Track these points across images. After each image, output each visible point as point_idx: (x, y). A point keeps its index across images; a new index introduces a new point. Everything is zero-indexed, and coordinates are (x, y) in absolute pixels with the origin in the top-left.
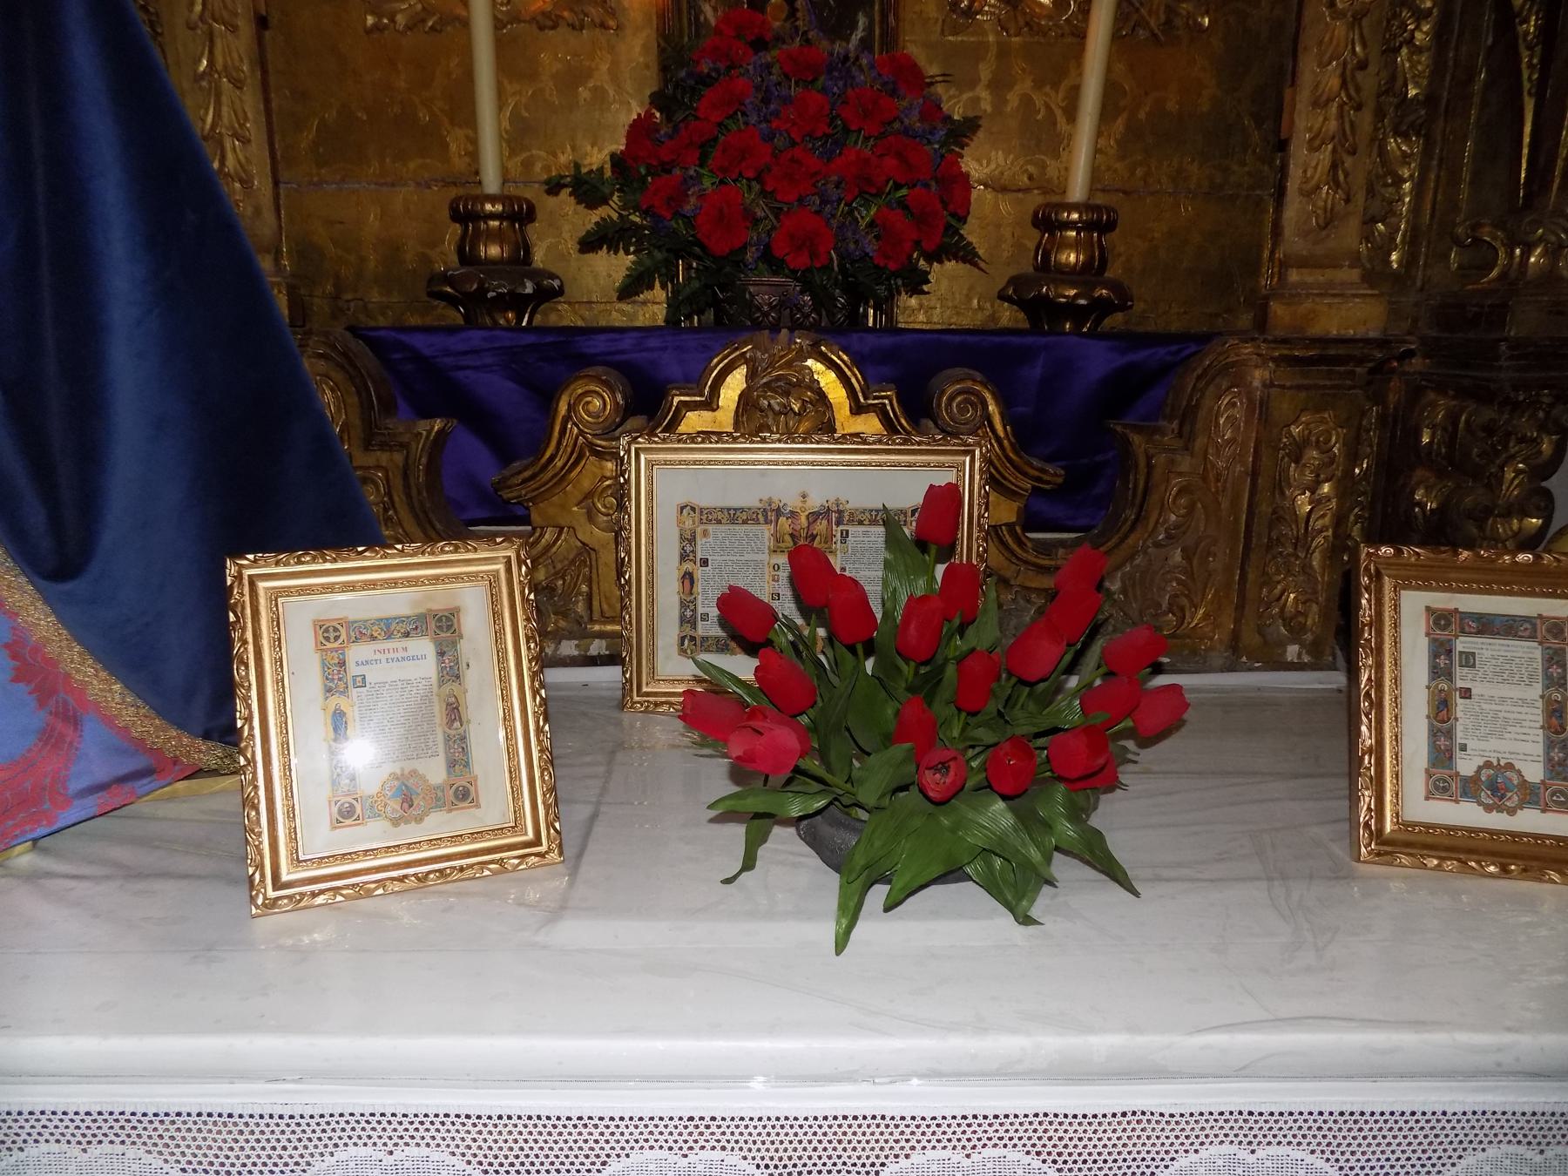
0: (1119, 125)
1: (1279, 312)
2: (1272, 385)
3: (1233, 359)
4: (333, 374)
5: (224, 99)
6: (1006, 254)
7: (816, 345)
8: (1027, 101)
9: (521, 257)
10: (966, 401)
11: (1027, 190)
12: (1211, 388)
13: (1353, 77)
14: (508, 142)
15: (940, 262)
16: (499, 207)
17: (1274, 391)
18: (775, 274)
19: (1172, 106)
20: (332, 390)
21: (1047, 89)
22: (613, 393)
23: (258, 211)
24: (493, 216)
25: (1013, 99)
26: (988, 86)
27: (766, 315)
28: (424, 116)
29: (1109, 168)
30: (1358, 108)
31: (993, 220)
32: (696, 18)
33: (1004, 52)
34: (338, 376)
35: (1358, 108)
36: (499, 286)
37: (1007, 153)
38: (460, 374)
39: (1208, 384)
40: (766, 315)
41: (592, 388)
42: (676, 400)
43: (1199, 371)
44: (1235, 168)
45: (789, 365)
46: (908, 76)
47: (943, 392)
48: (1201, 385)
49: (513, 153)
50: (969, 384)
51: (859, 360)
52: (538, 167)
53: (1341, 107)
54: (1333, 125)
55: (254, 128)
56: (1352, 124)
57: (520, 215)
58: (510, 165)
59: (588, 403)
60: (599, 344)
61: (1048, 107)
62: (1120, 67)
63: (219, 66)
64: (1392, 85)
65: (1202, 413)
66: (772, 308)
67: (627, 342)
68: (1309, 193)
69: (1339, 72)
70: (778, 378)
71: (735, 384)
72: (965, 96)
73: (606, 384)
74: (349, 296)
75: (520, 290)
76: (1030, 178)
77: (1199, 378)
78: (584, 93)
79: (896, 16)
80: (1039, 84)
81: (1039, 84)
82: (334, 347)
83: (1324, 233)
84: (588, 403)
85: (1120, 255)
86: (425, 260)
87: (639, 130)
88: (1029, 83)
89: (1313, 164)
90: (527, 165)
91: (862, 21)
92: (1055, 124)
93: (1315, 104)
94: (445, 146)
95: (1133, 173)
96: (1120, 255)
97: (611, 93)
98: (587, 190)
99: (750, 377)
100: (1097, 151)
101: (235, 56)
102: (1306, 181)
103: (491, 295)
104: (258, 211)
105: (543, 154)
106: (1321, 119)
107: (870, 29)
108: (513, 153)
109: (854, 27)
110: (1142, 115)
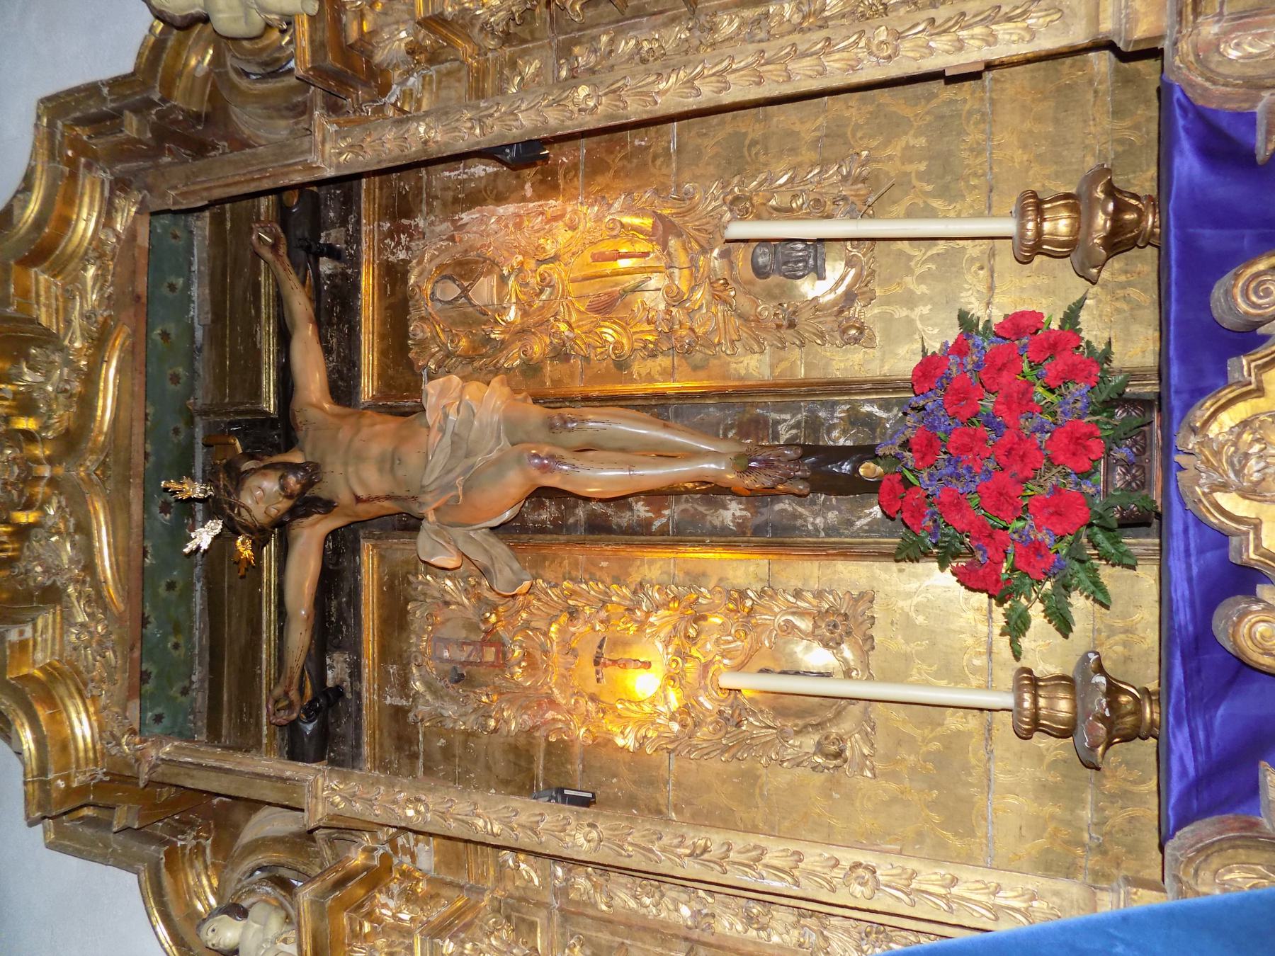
0: (937, 204)
1: (1145, 27)
2: (1221, 14)
3: (1192, 58)
4: (1214, 866)
5: (967, 895)
6: (1046, 281)
7: (1194, 431)
8: (922, 279)
9: (1066, 682)
10: (1256, 293)
11: (992, 272)
12: (1221, 70)
13: (940, 26)
14: (956, 683)
15: (1080, 330)
16: (1027, 696)
17: (1226, 11)
18: (1097, 470)
19: (922, 167)
20: (1231, 871)
21: (912, 264)
22: (1251, 613)
23: (1056, 893)
24: (1035, 702)
25: (922, 289)
26: (912, 309)
27: (1134, 477)
28: (936, 746)
29: (972, 207)
30: (963, 14)
31: (1042, 292)
32: (866, 531)
33: (887, 301)
34: (1215, 862)
35: (963, 14)
36: (1100, 704)
37: (962, 289)
38: (1214, 751)
39: (1219, 74)
40: (1134, 477)
41: (1246, 631)
42: (1252, 556)
43: (1208, 84)
44: (967, 107)
45: (1217, 454)
46: (929, 368)
47: (1247, 313)
48: (1221, 80)
49: (965, 680)
50: (1237, 292)
51: (1198, 393)
52: (977, 662)
53: (962, 28)
54: (978, 30)
55: (993, 878)
56: (975, 16)
57: (1029, 681)
58: (974, 683)
59: (1263, 637)
60: (1183, 616)
61: (924, 263)
62: (896, 209)
63: (943, 891)
64: (686, 49)
65: (1250, 72)
66: (1128, 471)
67: (1181, 590)
68: (1032, 33)
69: (937, 38)
70: (1232, 464)
71: (1229, 501)
72: (920, 326)
73: (1241, 618)
74: (1086, 836)
75: (1104, 688)
76: (982, 268)
77: (1214, 83)
78: (920, 620)
79: (865, 382)
80: (910, 271)
81: (910, 271)
82: (1190, 860)
83: (1066, 11)
84: (1263, 637)
85: (1043, 186)
86: (1054, 765)
87: (969, 580)
88: (908, 279)
89: (1007, 37)
90: (975, 671)
91: (867, 408)
92: (938, 254)
93: (960, 49)
94: (958, 734)
95: (975, 187)
96: (1043, 186)
97: (920, 599)
98: (1017, 626)
99: (1224, 487)
100: (958, 216)
101: (934, 877)
102: (1022, 39)
103: (1107, 714)
104: (1056, 893)
105: (966, 657)
106: (971, 42)
107: (871, 402)
108: (965, 680)
109: (870, 414)
110: (929, 188)
